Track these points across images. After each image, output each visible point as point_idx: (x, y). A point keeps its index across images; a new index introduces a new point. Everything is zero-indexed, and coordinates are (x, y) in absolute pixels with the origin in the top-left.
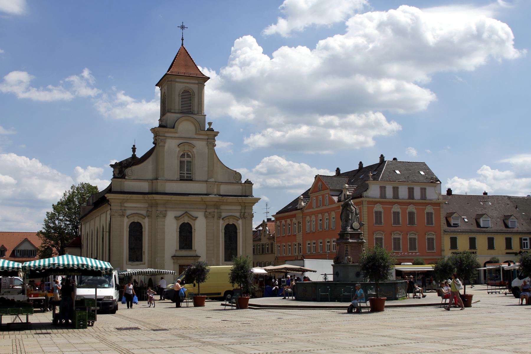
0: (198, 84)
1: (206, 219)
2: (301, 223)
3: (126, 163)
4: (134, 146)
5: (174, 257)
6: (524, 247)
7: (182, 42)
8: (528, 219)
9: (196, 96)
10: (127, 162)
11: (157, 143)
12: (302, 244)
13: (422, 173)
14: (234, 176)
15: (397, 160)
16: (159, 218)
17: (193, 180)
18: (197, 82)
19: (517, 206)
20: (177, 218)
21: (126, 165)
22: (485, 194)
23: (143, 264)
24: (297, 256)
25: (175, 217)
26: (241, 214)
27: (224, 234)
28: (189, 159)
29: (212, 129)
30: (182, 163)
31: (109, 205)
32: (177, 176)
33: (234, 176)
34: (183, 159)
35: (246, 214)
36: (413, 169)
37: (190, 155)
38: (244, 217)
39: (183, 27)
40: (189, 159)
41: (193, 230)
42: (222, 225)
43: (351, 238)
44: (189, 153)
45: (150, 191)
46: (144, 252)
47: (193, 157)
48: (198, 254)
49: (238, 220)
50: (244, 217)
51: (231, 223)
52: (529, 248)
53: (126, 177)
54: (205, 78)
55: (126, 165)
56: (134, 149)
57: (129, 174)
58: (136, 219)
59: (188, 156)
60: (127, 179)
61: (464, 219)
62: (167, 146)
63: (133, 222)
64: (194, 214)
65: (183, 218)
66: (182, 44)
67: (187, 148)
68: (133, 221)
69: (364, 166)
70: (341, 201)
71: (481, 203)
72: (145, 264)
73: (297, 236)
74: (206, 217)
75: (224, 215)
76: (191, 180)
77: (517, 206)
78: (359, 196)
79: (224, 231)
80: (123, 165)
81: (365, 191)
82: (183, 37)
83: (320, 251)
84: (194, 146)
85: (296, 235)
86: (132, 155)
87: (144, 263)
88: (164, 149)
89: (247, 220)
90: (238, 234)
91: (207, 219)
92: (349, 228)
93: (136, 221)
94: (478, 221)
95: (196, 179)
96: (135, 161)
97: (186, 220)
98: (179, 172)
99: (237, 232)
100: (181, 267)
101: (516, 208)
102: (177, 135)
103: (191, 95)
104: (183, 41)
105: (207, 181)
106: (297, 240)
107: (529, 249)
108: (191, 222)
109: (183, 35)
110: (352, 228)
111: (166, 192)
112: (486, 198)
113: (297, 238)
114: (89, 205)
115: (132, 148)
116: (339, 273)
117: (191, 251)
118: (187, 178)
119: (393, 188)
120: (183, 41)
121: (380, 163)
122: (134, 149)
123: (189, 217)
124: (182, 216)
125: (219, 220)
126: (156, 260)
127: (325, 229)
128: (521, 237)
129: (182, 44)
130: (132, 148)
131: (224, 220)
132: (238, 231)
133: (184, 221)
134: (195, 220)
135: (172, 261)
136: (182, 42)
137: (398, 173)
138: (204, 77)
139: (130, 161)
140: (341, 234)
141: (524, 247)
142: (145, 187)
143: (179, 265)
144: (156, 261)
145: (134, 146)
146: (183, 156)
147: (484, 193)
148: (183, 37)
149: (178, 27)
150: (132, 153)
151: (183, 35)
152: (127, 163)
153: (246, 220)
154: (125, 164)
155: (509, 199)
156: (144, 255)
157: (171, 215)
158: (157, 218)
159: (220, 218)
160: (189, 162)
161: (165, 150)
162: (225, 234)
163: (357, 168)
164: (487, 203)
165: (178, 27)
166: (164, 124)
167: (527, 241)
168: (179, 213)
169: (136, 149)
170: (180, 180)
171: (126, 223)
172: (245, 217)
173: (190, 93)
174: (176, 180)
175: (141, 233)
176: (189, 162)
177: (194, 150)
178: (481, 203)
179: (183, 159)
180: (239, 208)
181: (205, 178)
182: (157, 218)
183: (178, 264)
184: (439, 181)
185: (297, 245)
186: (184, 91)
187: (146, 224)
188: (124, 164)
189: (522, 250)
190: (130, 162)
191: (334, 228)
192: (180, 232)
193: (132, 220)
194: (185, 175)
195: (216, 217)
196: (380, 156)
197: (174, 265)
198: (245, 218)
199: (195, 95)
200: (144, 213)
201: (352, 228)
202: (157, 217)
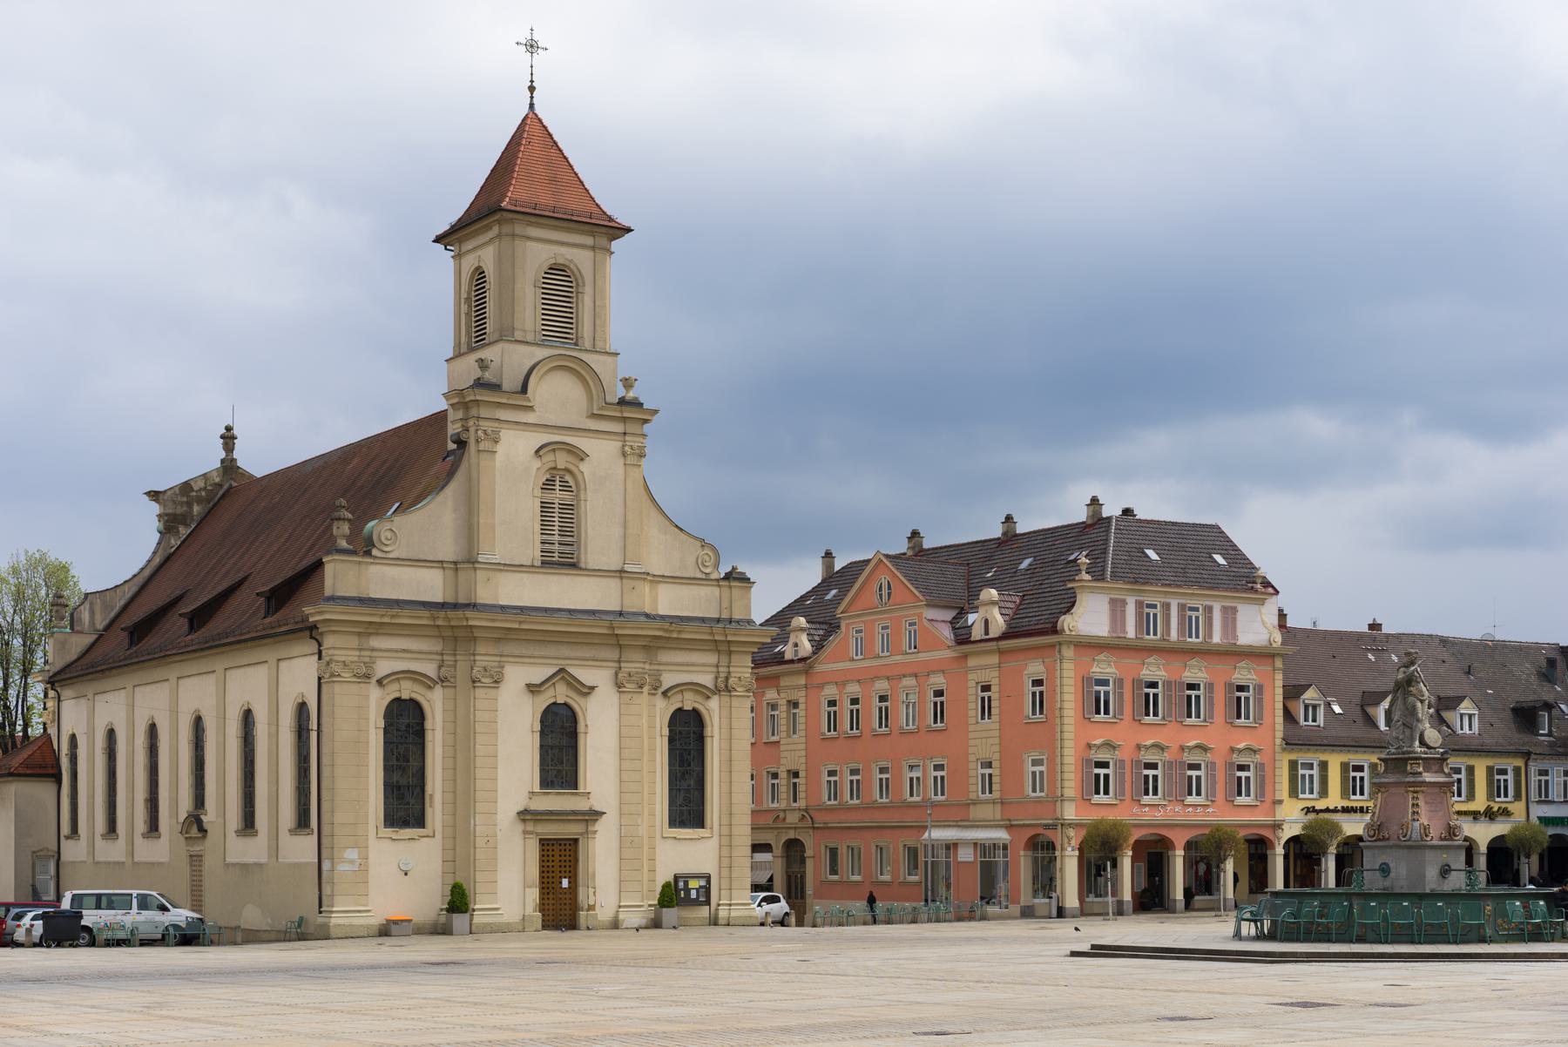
0: (593, 248)
1: (618, 694)
2: (802, 706)
3: (205, 489)
4: (229, 429)
5: (525, 815)
6: (1499, 796)
7: (532, 97)
8: (1504, 710)
9: (588, 289)
10: (205, 483)
11: (472, 441)
12: (802, 774)
13: (1219, 559)
14: (697, 559)
15: (1135, 516)
16: (478, 687)
17: (582, 565)
18: (589, 241)
19: (1470, 666)
20: (533, 689)
21: (203, 494)
22: (1374, 626)
23: (428, 836)
24: (784, 811)
25: (528, 686)
26: (717, 678)
27: (666, 740)
28: (566, 497)
29: (636, 398)
30: (545, 507)
31: (314, 641)
32: (533, 554)
33: (697, 559)
34: (549, 497)
35: (731, 681)
36: (1193, 546)
37: (571, 483)
38: (726, 686)
39: (532, 46)
40: (566, 497)
41: (581, 728)
42: (662, 711)
43: (1427, 770)
44: (568, 478)
45: (450, 599)
46: (431, 795)
47: (578, 491)
48: (595, 804)
49: (708, 697)
50: (726, 686)
51: (688, 707)
52: (1510, 798)
53: (375, 552)
54: (617, 228)
55: (203, 494)
56: (229, 438)
57: (383, 540)
58: (407, 690)
59: (566, 487)
60: (376, 557)
61: (1330, 704)
62: (501, 449)
63: (398, 700)
64: (585, 675)
65: (552, 689)
66: (532, 106)
67: (562, 460)
68: (397, 695)
69: (1020, 529)
70: (972, 639)
71: (1370, 656)
72: (434, 836)
73: (782, 748)
74: (619, 686)
75: (669, 680)
76: (574, 566)
77: (1470, 666)
78: (1050, 625)
79: (666, 732)
80: (194, 494)
81: (1065, 614)
82: (532, 81)
83: (827, 798)
84: (581, 456)
85: (778, 742)
86: (223, 461)
87: (431, 834)
88: (494, 461)
89: (478, 687)
90: (708, 742)
91: (620, 692)
92: (1417, 743)
93: (405, 696)
94: (1292, 710)
95: (591, 566)
96: (235, 484)
97: (561, 694)
98: (538, 538)
99: (578, 731)
100: (543, 845)
101: (1469, 673)
102: (530, 418)
103: (571, 282)
104: (532, 94)
105: (622, 571)
106: (783, 761)
107: (1513, 800)
108: (576, 702)
109: (532, 74)
110: (1423, 743)
111: (502, 602)
112: (1380, 641)
113: (782, 755)
114: (81, 632)
115: (222, 437)
116: (1391, 865)
117: (576, 794)
118: (560, 560)
119: (1109, 603)
120: (532, 94)
121: (1089, 522)
122: (229, 438)
123: (569, 684)
124: (551, 683)
125: (497, 688)
126: (472, 822)
127: (902, 728)
128: (1491, 764)
129: (532, 106)
130: (222, 437)
131: (669, 697)
132: (428, 725)
133: (555, 696)
134: (586, 695)
135: (520, 827)
136: (532, 97)
137: (1153, 558)
138: (616, 225)
139: (217, 480)
140: (1390, 759)
141: (1354, 794)
142: (430, 585)
143: (541, 840)
144: (472, 829)
145: (229, 429)
146: (548, 485)
147: (1369, 625)
148: (532, 81)
149: (517, 43)
150: (223, 454)
151: (532, 74)
152: (209, 488)
153: (731, 696)
154: (200, 490)
155: (1444, 647)
156: (431, 806)
157: (518, 676)
158: (474, 687)
159: (656, 689)
160: (567, 507)
161: (498, 464)
162: (671, 740)
163: (996, 532)
164: (1385, 655)
165: (517, 43)
166: (488, 376)
167: (1505, 777)
168: (539, 674)
169: (236, 438)
170: (543, 563)
171: (376, 702)
172: (730, 688)
173: (569, 277)
174: (529, 563)
175: (701, 739)
176: (567, 507)
177: (584, 467)
178: (1370, 656)
179: (549, 497)
180: (711, 658)
181: (615, 564)
182: (474, 687)
183: (537, 834)
184: (1273, 587)
185: (783, 775)
186: (550, 269)
187: (436, 705)
188: (196, 492)
189: (1492, 804)
190: (215, 484)
191: (911, 727)
192: (542, 733)
193: (392, 692)
194: (556, 547)
195: (646, 689)
196: (1089, 502)
197: (525, 838)
198: (730, 691)
199: (584, 285)
200: (429, 669)
201: (1423, 743)
202: (474, 682)
